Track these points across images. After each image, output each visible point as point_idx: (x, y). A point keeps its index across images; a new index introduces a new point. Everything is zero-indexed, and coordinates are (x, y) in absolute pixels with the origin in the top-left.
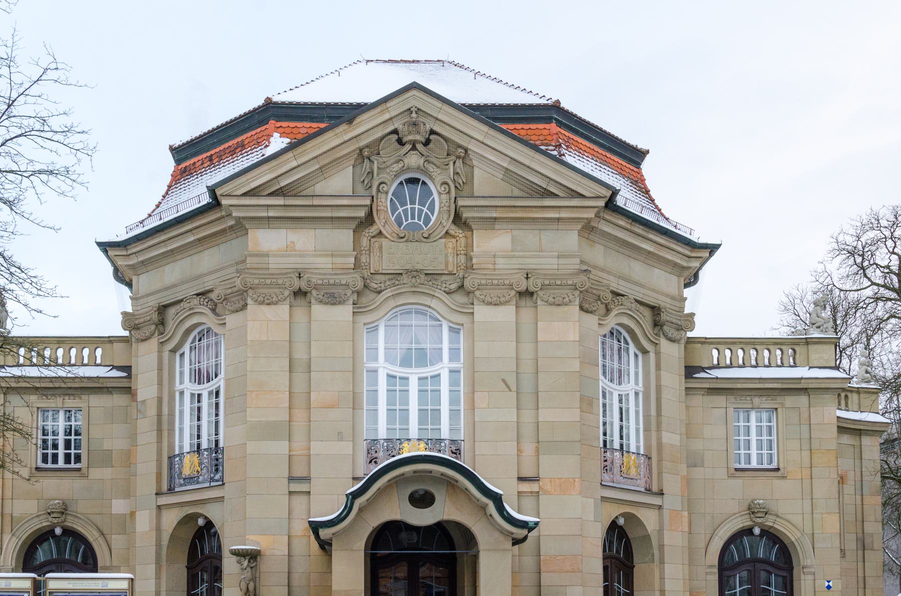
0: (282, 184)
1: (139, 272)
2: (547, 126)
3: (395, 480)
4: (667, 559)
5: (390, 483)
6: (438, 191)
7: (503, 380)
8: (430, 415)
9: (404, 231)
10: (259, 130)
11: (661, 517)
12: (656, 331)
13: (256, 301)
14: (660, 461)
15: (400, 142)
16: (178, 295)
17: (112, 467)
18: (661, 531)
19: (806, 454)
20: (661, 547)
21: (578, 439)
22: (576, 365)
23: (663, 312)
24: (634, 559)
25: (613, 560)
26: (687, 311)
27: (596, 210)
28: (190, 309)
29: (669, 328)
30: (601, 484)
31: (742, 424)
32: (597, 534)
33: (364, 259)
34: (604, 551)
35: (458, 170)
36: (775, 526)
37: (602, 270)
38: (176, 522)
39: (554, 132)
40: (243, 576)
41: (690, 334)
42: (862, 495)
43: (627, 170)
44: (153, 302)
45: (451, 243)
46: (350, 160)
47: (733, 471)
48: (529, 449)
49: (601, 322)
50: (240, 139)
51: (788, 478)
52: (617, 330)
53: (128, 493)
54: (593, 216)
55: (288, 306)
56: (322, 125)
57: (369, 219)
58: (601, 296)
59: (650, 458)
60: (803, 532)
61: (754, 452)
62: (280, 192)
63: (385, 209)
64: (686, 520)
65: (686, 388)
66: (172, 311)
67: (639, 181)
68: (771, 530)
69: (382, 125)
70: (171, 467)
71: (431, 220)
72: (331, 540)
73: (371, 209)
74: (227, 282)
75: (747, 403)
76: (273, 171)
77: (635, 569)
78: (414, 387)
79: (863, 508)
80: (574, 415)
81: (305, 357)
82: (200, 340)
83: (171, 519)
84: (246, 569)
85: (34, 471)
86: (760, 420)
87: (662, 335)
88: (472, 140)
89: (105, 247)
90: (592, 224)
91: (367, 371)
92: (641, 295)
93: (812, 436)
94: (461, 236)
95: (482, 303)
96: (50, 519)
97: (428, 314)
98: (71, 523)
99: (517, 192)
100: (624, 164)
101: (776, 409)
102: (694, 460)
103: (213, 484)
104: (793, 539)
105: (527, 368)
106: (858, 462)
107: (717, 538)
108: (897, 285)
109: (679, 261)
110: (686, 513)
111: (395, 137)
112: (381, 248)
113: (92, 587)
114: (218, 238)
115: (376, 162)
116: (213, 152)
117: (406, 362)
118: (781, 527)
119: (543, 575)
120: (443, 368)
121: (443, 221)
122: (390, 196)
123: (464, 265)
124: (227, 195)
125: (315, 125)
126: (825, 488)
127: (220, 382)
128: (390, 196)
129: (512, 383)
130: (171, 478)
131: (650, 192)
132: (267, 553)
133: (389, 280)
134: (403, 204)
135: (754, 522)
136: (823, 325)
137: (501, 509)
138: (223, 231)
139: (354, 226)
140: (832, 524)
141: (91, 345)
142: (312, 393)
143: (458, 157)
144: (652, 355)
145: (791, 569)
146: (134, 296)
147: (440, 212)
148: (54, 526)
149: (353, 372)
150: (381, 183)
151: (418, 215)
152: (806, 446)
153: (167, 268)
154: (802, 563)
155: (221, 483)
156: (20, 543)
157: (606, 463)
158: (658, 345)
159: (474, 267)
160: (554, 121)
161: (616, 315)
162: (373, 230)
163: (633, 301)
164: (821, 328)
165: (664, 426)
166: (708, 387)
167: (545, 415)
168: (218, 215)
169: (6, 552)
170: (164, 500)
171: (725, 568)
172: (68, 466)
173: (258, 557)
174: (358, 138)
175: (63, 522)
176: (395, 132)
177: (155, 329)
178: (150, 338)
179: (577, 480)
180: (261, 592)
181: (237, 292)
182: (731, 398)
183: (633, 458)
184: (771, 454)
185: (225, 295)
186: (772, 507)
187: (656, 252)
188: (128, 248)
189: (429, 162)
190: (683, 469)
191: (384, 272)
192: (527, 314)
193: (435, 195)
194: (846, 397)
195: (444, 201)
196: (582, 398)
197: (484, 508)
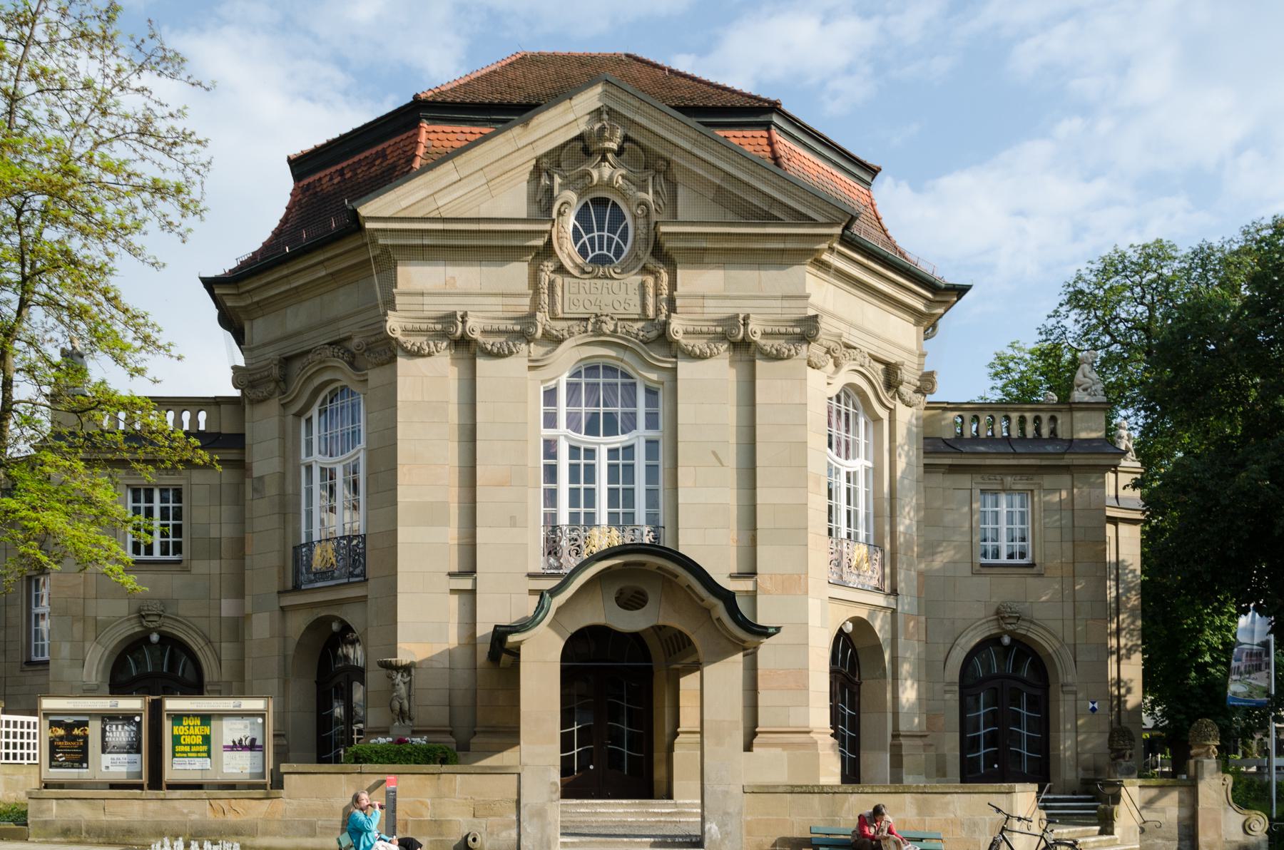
7: (714, 453)
10: (404, 136)
12: (891, 394)
28: (321, 362)
31: (989, 509)
36: (1029, 634)
38: (304, 627)
43: (856, 192)
44: (271, 354)
47: (977, 567)
49: (830, 381)
50: (379, 148)
51: (1046, 575)
56: (486, 130)
60: (1062, 642)
65: (925, 465)
66: (297, 366)
68: (1023, 640)
74: (369, 328)
78: (602, 463)
82: (331, 402)
83: (298, 624)
86: (1011, 505)
87: (897, 399)
92: (875, 348)
98: (169, 628)
103: (351, 580)
104: (1050, 651)
108: (199, 444)
111: (579, 145)
116: (344, 164)
117: (592, 429)
118: (1036, 635)
121: (640, 253)
125: (476, 130)
130: (297, 572)
134: (589, 230)
135: (1003, 629)
136: (1091, 387)
141: (193, 407)
145: (1046, 687)
151: (607, 244)
153: (289, 311)
154: (1061, 680)
155: (363, 579)
163: (867, 356)
164: (1089, 390)
170: (289, 600)
174: (534, 145)
178: (269, 399)
181: (383, 340)
182: (978, 478)
185: (367, 345)
193: (629, 220)
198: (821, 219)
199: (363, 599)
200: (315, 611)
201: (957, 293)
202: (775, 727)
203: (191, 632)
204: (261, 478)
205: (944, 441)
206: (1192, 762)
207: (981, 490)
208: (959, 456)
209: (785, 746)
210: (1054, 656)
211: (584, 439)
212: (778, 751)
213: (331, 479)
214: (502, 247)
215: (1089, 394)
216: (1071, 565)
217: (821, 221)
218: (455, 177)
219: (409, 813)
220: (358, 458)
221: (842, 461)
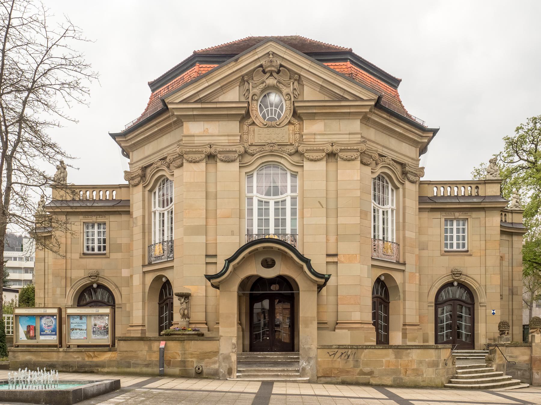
0: (201, 96)
1: (134, 149)
2: (345, 63)
3: (253, 253)
4: (407, 298)
5: (250, 254)
6: (284, 99)
7: (319, 202)
8: (280, 222)
9: (267, 122)
11: (404, 276)
13: (188, 161)
14: (404, 246)
15: (264, 72)
16: (151, 161)
17: (122, 252)
18: (404, 283)
19: (483, 243)
20: (404, 292)
21: (359, 233)
22: (358, 193)
23: (407, 166)
24: (390, 298)
25: (378, 299)
26: (420, 166)
27: (370, 107)
29: (410, 175)
30: (371, 258)
31: (449, 227)
32: (369, 285)
33: (245, 137)
34: (373, 293)
35: (295, 87)
36: (466, 281)
37: (374, 142)
39: (349, 66)
40: (182, 307)
41: (422, 179)
42: (512, 266)
45: (291, 127)
46: (238, 83)
47: (443, 252)
48: (332, 239)
51: (473, 255)
52: (382, 176)
53: (129, 265)
54: (368, 110)
55: (205, 163)
57: (247, 115)
58: (373, 156)
59: (399, 245)
61: (455, 242)
62: (199, 101)
63: (256, 109)
64: (417, 278)
65: (419, 208)
66: (149, 170)
67: (396, 96)
69: (254, 63)
70: (149, 252)
71: (281, 116)
72: (219, 286)
73: (249, 109)
75: (451, 216)
76: (195, 89)
77: (390, 304)
79: (512, 273)
80: (357, 220)
81: (214, 191)
83: (150, 278)
84: (183, 303)
85: (82, 255)
87: (406, 179)
88: (303, 70)
89: (114, 136)
90: (368, 116)
91: (248, 199)
93: (486, 233)
94: (297, 123)
95: (308, 160)
96: (90, 279)
97: (280, 167)
98: (101, 281)
99: (327, 99)
100: (388, 86)
101: (467, 219)
102: (423, 247)
104: (475, 288)
105: (332, 195)
106: (510, 249)
107: (434, 287)
109: (416, 139)
110: (418, 274)
112: (254, 131)
113: (90, 312)
114: (169, 128)
115: (251, 83)
116: (169, 84)
117: (268, 194)
118: (468, 281)
119: (339, 306)
120: (287, 196)
122: (259, 103)
123: (299, 139)
124: (170, 103)
126: (493, 260)
127: (172, 206)
128: (259, 103)
129: (324, 203)
131: (402, 103)
132: (194, 295)
133: (258, 148)
135: (454, 279)
137: (310, 268)
138: (170, 125)
139: (239, 119)
140: (496, 280)
142: (218, 210)
143: (295, 80)
144: (401, 190)
145: (473, 304)
146: (490, 362)
147: (286, 110)
148: (93, 283)
149: (240, 198)
150: (253, 95)
152: (483, 238)
154: (479, 301)
155: (173, 259)
156: (75, 292)
157: (375, 247)
158: (404, 185)
159: (304, 141)
160: (349, 61)
161: (381, 167)
162: (249, 121)
164: (493, 174)
165: (407, 228)
166: (431, 207)
167: (341, 220)
168: (168, 115)
169: (68, 297)
170: (146, 269)
171: (438, 304)
172: (100, 252)
173: (190, 297)
175: (97, 281)
176: (261, 66)
177: (141, 180)
178: (139, 184)
179: (358, 255)
180: (191, 316)
182: (444, 214)
183: (389, 244)
184: (464, 243)
186: (464, 272)
187: (404, 133)
188: (126, 136)
189: (280, 83)
190: (417, 251)
191: (256, 144)
192: (332, 166)
194: (505, 215)
195: (288, 104)
196: (361, 212)
197: (301, 268)
198: (350, 99)
199: (172, 267)
200: (156, 273)
201: (433, 132)
202: (345, 321)
203: (109, 283)
204: (136, 218)
205: (428, 197)
206: (530, 335)
207: (445, 219)
208: (435, 204)
209: (349, 329)
210: (476, 290)
211: (264, 198)
212: (346, 331)
213: (163, 217)
214: (227, 115)
215: (493, 176)
216: (485, 251)
217: (365, 99)
218: (206, 85)
219: (171, 357)
220: (172, 209)
221: (380, 206)
